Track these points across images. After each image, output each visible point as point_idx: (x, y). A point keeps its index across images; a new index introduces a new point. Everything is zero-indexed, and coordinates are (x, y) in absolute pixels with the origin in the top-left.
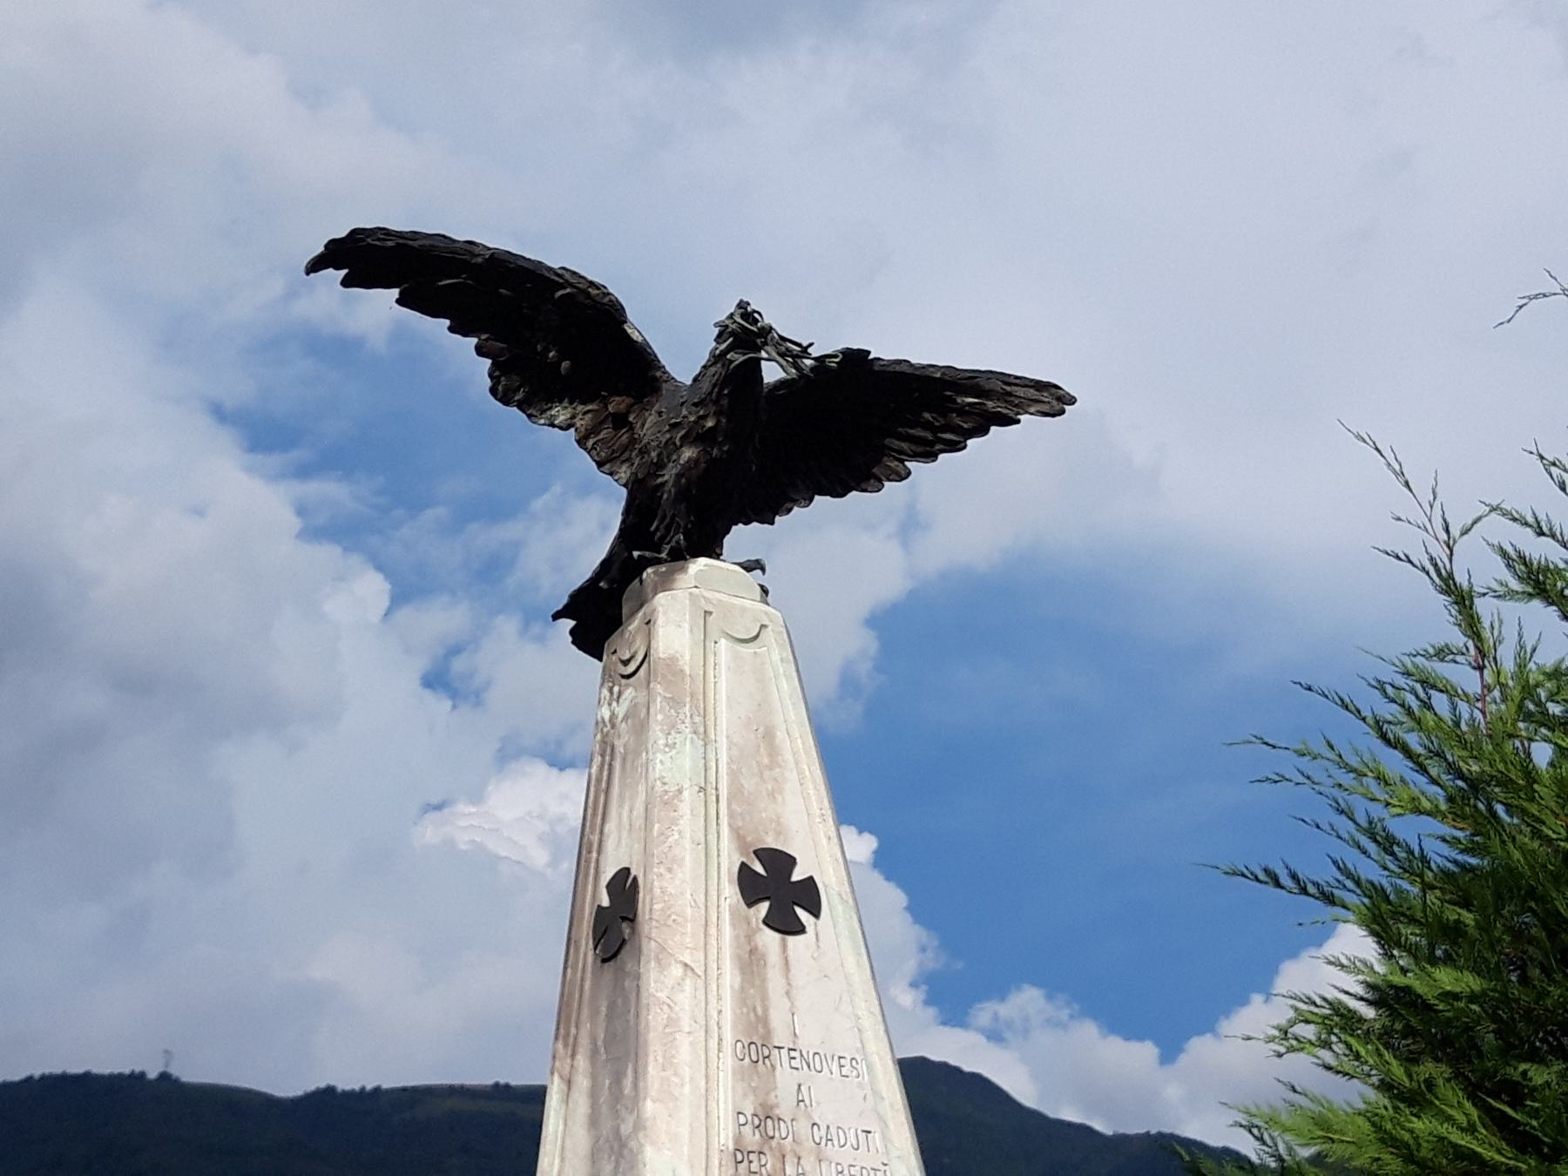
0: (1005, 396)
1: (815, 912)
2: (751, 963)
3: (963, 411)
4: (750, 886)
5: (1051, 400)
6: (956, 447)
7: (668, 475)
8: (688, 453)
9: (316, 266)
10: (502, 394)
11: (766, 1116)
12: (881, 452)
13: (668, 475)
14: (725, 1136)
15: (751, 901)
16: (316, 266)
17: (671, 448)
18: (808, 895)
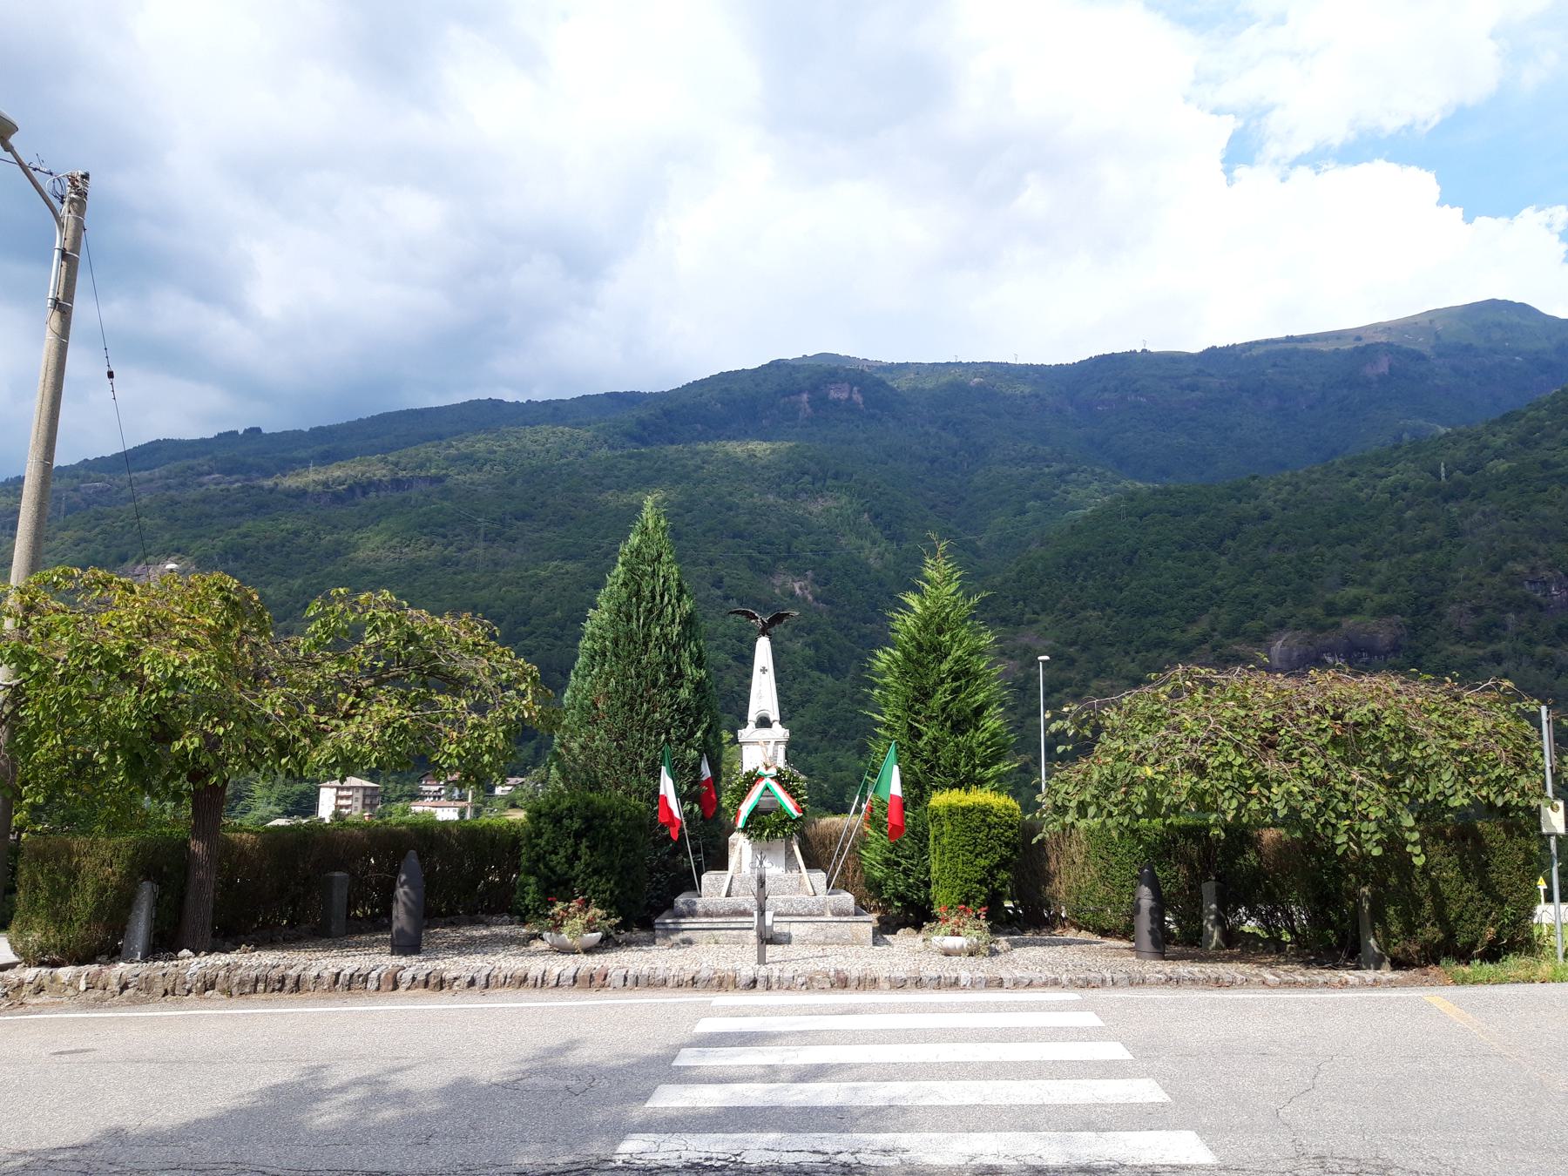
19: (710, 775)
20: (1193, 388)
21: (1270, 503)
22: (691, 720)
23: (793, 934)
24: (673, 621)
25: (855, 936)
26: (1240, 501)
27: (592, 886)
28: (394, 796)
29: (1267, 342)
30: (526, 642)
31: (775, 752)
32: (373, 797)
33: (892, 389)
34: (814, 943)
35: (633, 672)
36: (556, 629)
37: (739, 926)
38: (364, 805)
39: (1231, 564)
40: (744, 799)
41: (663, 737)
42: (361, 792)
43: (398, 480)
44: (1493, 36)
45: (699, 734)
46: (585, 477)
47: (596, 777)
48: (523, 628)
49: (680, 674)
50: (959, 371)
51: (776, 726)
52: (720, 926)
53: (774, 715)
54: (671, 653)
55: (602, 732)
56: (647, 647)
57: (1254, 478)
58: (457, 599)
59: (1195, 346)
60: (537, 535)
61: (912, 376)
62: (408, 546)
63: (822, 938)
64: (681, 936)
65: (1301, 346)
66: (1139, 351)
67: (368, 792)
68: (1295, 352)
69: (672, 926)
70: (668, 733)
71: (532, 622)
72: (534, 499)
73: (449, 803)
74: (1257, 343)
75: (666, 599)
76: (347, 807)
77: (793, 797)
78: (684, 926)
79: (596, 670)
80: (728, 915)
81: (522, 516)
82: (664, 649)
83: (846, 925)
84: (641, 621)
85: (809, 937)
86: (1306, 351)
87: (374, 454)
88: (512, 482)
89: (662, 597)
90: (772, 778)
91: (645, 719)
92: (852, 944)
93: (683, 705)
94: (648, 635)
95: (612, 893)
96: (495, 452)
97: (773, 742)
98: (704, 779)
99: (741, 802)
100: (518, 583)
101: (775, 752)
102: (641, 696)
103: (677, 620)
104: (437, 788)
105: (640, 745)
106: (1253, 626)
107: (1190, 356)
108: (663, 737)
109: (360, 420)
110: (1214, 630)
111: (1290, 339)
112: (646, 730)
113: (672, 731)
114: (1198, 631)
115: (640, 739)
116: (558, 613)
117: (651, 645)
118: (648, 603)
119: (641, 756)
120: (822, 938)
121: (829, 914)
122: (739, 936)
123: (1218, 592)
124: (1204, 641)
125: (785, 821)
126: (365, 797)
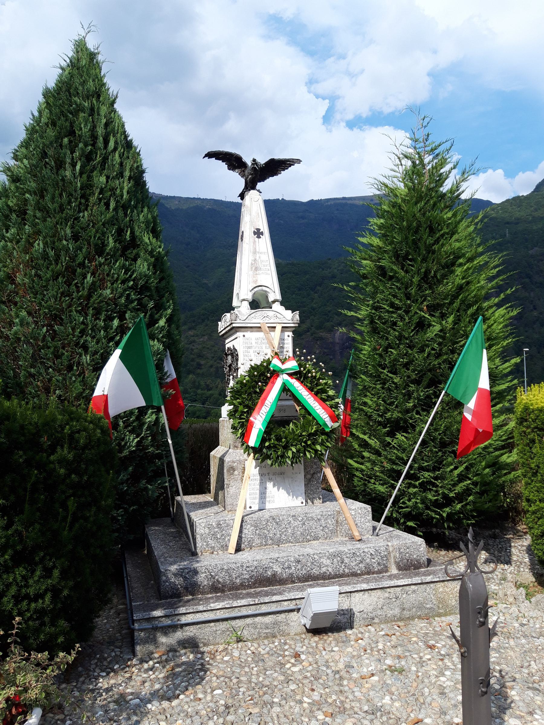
0: (293, 162)
1: (263, 235)
2: (254, 242)
3: (288, 164)
4: (255, 233)
5: (299, 161)
6: (287, 169)
7: (248, 179)
8: (250, 176)
9: (204, 157)
10: (229, 169)
11: (255, 260)
12: (278, 170)
13: (248, 179)
14: (250, 262)
15: (255, 235)
16: (204, 157)
17: (248, 176)
18: (262, 233)
19: (175, 377)
20: (303, 218)
21: (335, 271)
22: (151, 304)
23: (356, 610)
24: (121, 175)
25: (442, 601)
26: (323, 270)
27: (13, 590)
29: (335, 199)
31: (282, 340)
33: (167, 208)
34: (386, 620)
35: (68, 231)
37: (274, 608)
39: (319, 297)
40: (255, 405)
41: (116, 322)
44: (429, 75)
45: (162, 322)
47: (16, 375)
49: (134, 243)
50: (199, 202)
51: (277, 307)
52: (244, 612)
53: (275, 294)
54: (121, 213)
55: (24, 313)
56: (87, 200)
57: (330, 259)
59: (305, 199)
61: (177, 203)
63: (397, 611)
64: (179, 635)
65: (349, 202)
66: (280, 199)
68: (346, 204)
69: (167, 622)
70: (122, 318)
74: (330, 199)
75: (112, 144)
77: (324, 400)
78: (184, 620)
79: (13, 231)
82: (112, 205)
83: (428, 588)
84: (78, 167)
85: (379, 612)
86: (350, 204)
89: (106, 142)
90: (290, 375)
91: (89, 297)
92: (440, 615)
93: (141, 283)
94: (88, 186)
95: (55, 591)
97: (279, 328)
98: (168, 380)
99: (250, 410)
101: (282, 340)
102: (82, 265)
103: (127, 174)
105: (83, 332)
106: (328, 324)
107: (302, 203)
108: (116, 322)
110: (312, 326)
111: (344, 198)
112: (91, 311)
113: (127, 316)
114: (306, 326)
115: (83, 323)
117: (93, 199)
118: (86, 145)
119: (85, 348)
120: (397, 611)
121: (394, 570)
122: (276, 623)
123: (314, 309)
124: (308, 331)
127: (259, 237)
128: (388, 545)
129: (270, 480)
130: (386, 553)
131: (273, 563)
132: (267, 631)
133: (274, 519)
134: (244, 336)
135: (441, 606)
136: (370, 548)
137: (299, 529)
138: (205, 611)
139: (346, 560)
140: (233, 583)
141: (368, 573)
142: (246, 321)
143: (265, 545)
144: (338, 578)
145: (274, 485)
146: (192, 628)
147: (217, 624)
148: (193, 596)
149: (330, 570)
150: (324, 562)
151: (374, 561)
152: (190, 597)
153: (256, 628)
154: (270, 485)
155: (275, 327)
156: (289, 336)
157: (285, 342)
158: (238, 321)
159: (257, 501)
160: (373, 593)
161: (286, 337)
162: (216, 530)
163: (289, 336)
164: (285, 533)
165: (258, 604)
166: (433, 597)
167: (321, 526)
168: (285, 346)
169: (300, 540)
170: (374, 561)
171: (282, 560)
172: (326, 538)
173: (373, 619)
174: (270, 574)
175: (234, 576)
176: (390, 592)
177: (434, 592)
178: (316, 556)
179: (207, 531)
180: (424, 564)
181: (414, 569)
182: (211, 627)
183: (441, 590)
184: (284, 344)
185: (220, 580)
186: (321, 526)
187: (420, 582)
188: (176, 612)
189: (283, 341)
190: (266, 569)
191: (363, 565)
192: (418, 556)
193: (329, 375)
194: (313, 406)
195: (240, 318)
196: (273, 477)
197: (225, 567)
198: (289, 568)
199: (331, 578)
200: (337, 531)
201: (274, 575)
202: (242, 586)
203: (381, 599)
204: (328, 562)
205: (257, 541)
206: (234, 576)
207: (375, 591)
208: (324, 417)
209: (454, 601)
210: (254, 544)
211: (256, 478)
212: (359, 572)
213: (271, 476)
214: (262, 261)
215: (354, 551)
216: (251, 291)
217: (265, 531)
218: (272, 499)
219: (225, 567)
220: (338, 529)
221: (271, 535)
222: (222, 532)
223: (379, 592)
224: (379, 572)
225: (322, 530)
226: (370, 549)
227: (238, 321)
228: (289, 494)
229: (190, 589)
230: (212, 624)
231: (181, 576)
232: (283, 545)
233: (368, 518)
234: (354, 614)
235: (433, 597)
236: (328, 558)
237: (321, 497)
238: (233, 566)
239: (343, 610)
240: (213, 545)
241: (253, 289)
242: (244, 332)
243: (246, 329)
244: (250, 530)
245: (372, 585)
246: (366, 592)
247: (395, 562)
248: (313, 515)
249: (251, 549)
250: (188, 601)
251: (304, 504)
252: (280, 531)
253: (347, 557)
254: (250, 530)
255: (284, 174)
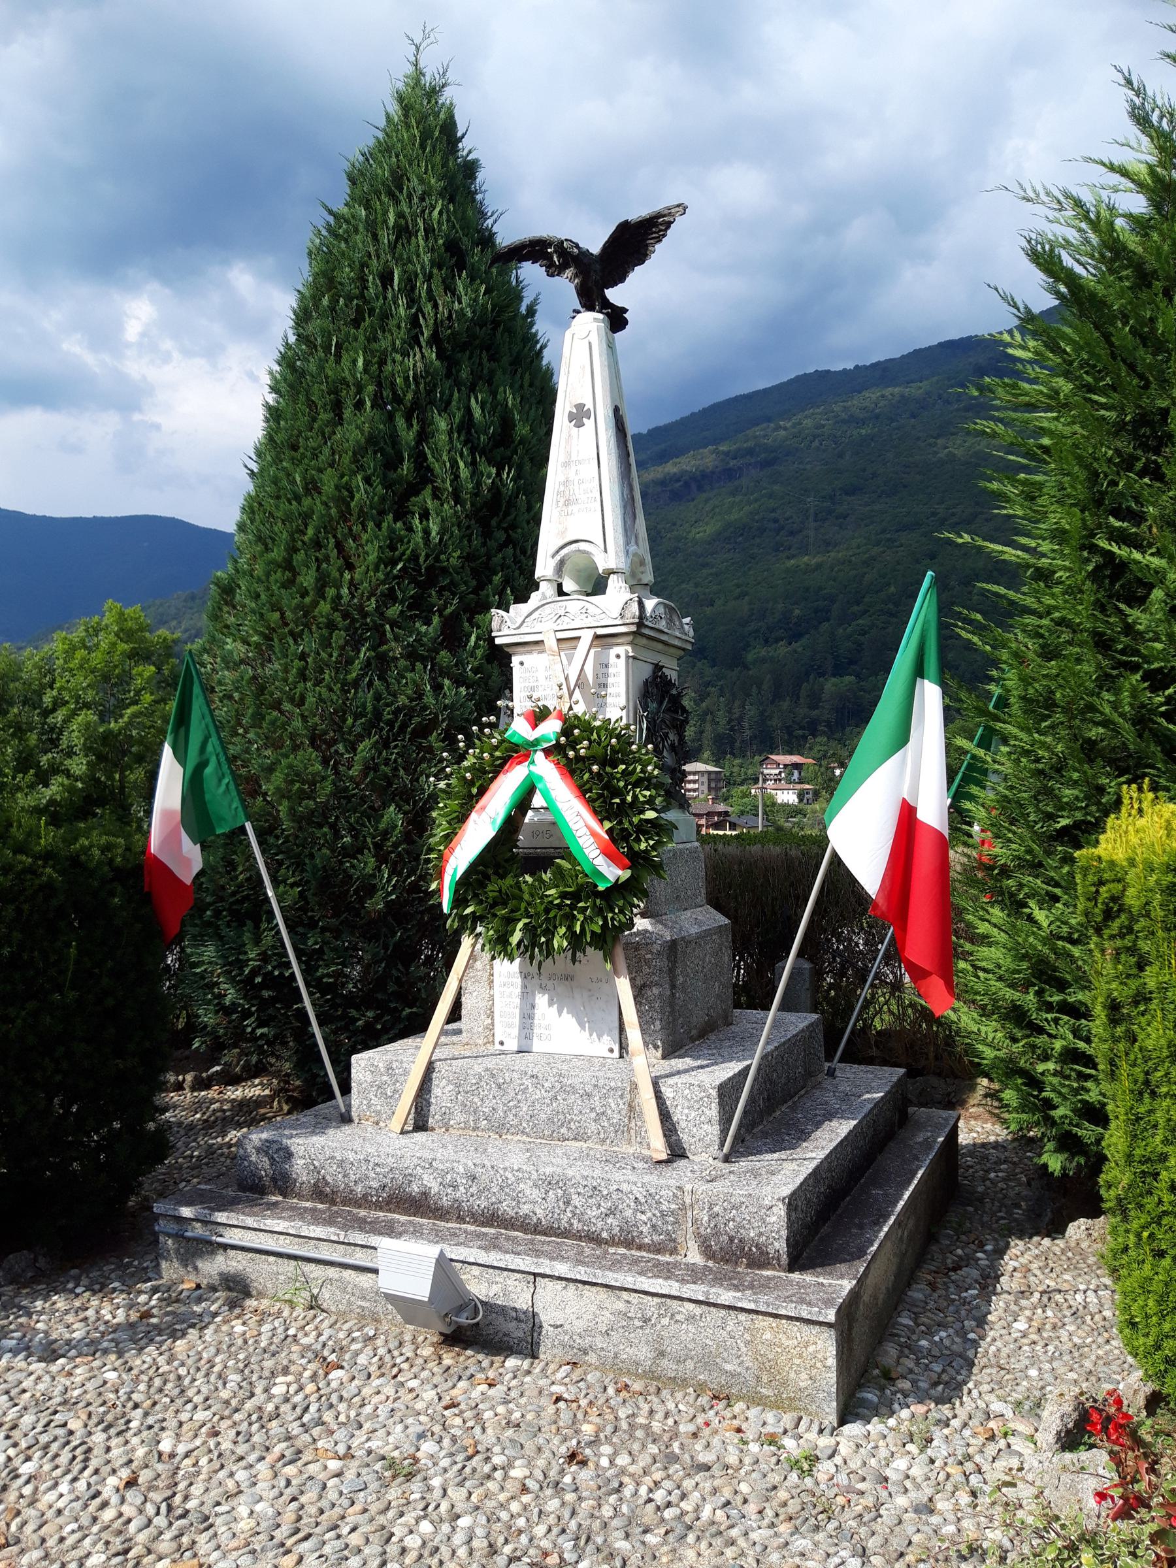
12: (647, 246)
23: (546, 1317)
25: (768, 1367)
28: (739, 779)
30: (860, 622)
32: (718, 780)
36: (891, 606)
38: (710, 789)
42: (706, 776)
43: (730, 469)
46: (918, 439)
48: (855, 608)
49: (424, 475)
52: (325, 1253)
53: (608, 558)
58: (789, 583)
60: (868, 508)
62: (742, 535)
67: (713, 776)
71: (866, 600)
72: (864, 470)
73: (788, 786)
76: (695, 790)
80: (378, 1206)
81: (852, 491)
83: (732, 1319)
85: (600, 1342)
87: (705, 447)
88: (841, 456)
96: (823, 426)
97: (587, 637)
100: (850, 562)
104: (777, 771)
109: (693, 414)
116: (892, 589)
120: (644, 1353)
125: (576, 897)
126: (710, 780)
127: (580, 425)
128: (680, 1188)
129: (543, 988)
130: (673, 1206)
131: (424, 1168)
132: (364, 1304)
133: (493, 1076)
134: (522, 663)
135: (765, 1379)
136: (635, 1184)
137: (545, 1107)
138: (255, 1229)
139: (576, 1200)
140: (352, 1191)
141: (628, 1244)
142: (523, 630)
143: (474, 1130)
144: (558, 1236)
145: (551, 1004)
146: (241, 1255)
147: (280, 1260)
148: (285, 1197)
149: (538, 1211)
150: (528, 1192)
151: (644, 1218)
152: (280, 1198)
153: (344, 1290)
154: (542, 1000)
155: (579, 638)
156: (618, 656)
157: (611, 670)
158: (505, 631)
159: (515, 1031)
160: (588, 1291)
161: (612, 659)
162: (385, 1078)
163: (618, 656)
164: (514, 1111)
165: (349, 1244)
166: (744, 1350)
167: (592, 1109)
168: (610, 680)
169: (546, 1133)
170: (644, 1218)
171: (441, 1167)
172: (604, 1141)
173: (586, 1354)
174: (416, 1189)
175: (353, 1177)
176: (628, 1302)
177: (747, 1336)
178: (510, 1176)
179: (369, 1078)
180: (779, 1260)
181: (749, 1266)
182: (269, 1264)
183: (768, 1336)
184: (606, 675)
185: (328, 1178)
186: (592, 1109)
187: (701, 1298)
188: (213, 1219)
189: (604, 670)
190: (409, 1178)
191: (615, 1223)
192: (761, 1234)
193: (566, 756)
194: (574, 827)
195: (509, 623)
196: (550, 983)
197: (338, 1156)
198: (455, 1187)
199: (540, 1233)
200: (629, 1129)
201: (425, 1194)
202: (364, 1201)
203: (605, 1312)
204: (536, 1194)
205: (458, 1118)
206: (353, 1177)
207: (594, 1289)
208: (592, 855)
209: (804, 1376)
210: (452, 1122)
211: (515, 980)
212: (605, 1235)
213: (545, 981)
214: (581, 482)
215: (595, 1184)
216: (553, 557)
217: (476, 1100)
218: (547, 1032)
219: (338, 1156)
220: (633, 1125)
221: (486, 1110)
222: (394, 1084)
223: (603, 1294)
224: (657, 1249)
225: (595, 1121)
226: (634, 1187)
227: (505, 631)
228: (583, 1027)
229: (279, 1183)
230: (272, 1259)
231: (267, 1153)
232: (509, 1137)
233: (707, 1112)
234: (541, 1327)
235: (744, 1350)
236: (536, 1186)
237: (659, 1043)
238: (351, 1156)
239: (515, 1309)
240: (379, 1108)
241: (557, 552)
242: (521, 654)
243: (527, 648)
244: (446, 1091)
245: (581, 1273)
246: (571, 1285)
247: (698, 1235)
248: (575, 1081)
249: (447, 1130)
250: (276, 1204)
251: (616, 1054)
252: (505, 1105)
253: (579, 1194)
254: (446, 1091)
255: (661, 252)
